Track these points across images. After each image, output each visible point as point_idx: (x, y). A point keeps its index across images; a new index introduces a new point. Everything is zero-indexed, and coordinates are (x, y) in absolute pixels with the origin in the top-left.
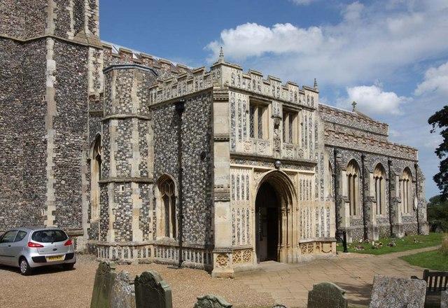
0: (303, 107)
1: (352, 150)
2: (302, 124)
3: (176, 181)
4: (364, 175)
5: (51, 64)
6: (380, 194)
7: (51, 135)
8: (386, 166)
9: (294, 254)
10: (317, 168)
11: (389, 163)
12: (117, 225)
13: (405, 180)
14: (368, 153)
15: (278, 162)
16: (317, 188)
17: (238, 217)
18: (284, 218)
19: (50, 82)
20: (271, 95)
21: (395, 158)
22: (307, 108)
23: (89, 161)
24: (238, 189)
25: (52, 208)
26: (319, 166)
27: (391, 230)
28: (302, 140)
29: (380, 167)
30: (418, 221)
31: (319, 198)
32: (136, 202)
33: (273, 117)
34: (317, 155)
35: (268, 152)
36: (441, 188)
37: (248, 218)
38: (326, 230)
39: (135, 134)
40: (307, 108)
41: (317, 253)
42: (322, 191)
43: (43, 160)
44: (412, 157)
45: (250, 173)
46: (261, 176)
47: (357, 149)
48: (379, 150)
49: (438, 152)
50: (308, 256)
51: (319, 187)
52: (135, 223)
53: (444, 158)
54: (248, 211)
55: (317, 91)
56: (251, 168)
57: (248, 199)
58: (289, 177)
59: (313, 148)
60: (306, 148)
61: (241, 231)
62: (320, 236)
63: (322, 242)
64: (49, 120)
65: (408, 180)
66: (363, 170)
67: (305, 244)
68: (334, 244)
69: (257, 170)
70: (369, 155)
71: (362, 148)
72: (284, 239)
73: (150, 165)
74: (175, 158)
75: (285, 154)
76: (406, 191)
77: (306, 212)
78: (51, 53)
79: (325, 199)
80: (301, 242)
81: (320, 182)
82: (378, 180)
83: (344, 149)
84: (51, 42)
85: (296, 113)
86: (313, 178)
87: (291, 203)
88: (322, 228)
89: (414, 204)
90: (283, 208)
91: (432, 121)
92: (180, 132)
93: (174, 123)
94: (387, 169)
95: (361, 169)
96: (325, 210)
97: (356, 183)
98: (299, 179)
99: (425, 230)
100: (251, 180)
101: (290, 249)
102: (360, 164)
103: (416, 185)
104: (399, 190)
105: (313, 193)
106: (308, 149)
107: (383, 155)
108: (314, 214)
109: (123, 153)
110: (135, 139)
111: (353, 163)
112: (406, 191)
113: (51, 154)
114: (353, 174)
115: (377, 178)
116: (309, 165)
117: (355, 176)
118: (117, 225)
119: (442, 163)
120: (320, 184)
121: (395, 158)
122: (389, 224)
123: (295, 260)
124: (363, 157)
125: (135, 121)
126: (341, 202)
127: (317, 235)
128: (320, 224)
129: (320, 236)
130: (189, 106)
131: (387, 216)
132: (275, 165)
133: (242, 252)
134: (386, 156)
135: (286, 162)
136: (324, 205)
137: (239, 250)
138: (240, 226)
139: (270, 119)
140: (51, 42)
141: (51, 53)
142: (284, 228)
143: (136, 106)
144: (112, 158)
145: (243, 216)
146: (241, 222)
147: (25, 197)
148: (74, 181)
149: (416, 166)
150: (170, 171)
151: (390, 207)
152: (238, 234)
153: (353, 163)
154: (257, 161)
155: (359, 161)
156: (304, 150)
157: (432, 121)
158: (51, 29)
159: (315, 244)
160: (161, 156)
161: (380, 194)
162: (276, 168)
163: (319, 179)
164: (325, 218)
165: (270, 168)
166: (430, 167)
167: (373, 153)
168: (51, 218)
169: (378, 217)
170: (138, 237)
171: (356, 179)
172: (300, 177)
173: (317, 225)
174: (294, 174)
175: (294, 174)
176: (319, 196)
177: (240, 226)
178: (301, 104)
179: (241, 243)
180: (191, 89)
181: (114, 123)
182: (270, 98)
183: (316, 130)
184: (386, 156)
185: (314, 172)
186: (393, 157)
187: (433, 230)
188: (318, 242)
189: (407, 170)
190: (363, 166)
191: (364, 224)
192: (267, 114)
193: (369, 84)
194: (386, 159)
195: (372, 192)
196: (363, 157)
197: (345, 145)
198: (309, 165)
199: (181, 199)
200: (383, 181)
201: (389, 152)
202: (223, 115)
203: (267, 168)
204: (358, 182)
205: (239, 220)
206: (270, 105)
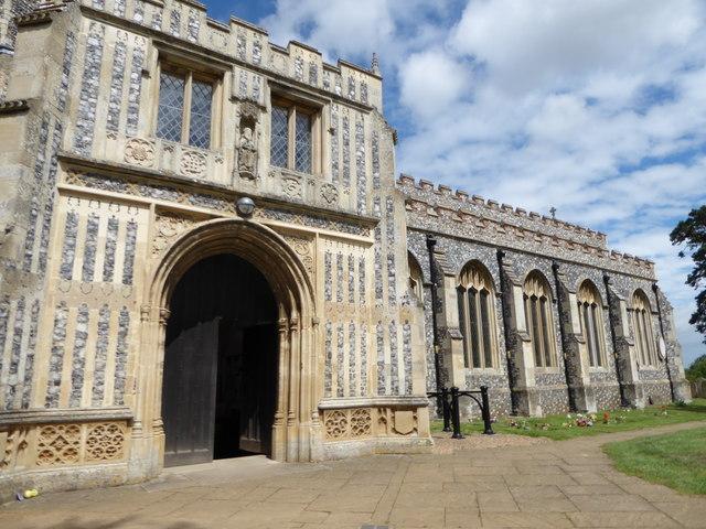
0: (336, 98)
1: (534, 255)
2: (332, 131)
4: (561, 296)
6: (596, 332)
8: (600, 285)
9: (304, 438)
10: (378, 232)
13: (638, 311)
14: (565, 261)
15: (247, 201)
16: (378, 276)
17: (82, 328)
18: (284, 344)
20: (232, 52)
21: (616, 273)
22: (348, 102)
24: (89, 253)
26: (383, 226)
27: (622, 393)
28: (335, 166)
29: (588, 285)
30: (669, 379)
31: (385, 301)
33: (234, 99)
34: (377, 201)
35: (219, 172)
37: (123, 335)
38: (402, 375)
40: (348, 102)
41: (379, 437)
42: (392, 284)
44: (645, 273)
45: (144, 217)
46: (182, 229)
47: (542, 253)
48: (585, 259)
49: (692, 280)
50: (349, 445)
51: (384, 273)
53: (701, 289)
54: (125, 314)
55: (377, 74)
56: (147, 205)
57: (128, 280)
58: (292, 245)
59: (369, 187)
60: (348, 184)
61: (89, 368)
62: (388, 391)
63: (394, 408)
65: (643, 311)
66: (558, 288)
67: (337, 411)
68: (424, 414)
69: (163, 212)
70: (566, 265)
71: (553, 252)
72: (282, 398)
76: (642, 329)
77: (347, 332)
79: (399, 301)
80: (325, 405)
81: (385, 262)
82: (589, 308)
83: (517, 251)
85: (317, 110)
86: (369, 254)
87: (299, 308)
88: (394, 373)
89: (659, 350)
90: (283, 319)
94: (603, 291)
95: (554, 287)
96: (400, 330)
97: (547, 312)
98: (320, 253)
101: (294, 424)
102: (551, 279)
103: (660, 319)
104: (627, 325)
105: (370, 289)
106: (354, 189)
107: (593, 267)
108: (371, 339)
111: (535, 276)
112: (642, 329)
114: (540, 294)
115: (586, 305)
117: (543, 300)
120: (385, 268)
121: (616, 273)
122: (616, 384)
123: (304, 454)
124: (555, 268)
126: (515, 342)
127: (381, 390)
128: (388, 361)
129: (388, 391)
131: (611, 369)
132: (237, 209)
133: (85, 432)
134: (599, 269)
136: (396, 317)
137: (73, 424)
138: (89, 352)
139: (228, 104)
142: (283, 370)
145: (104, 327)
146: (91, 343)
149: (655, 288)
152: (77, 377)
153: (535, 276)
154: (171, 189)
155: (548, 275)
156: (341, 189)
157: (676, 236)
159: (374, 414)
161: (596, 332)
162: (239, 214)
163: (384, 254)
164: (400, 345)
165: (216, 213)
166: (683, 303)
167: (574, 263)
169: (594, 372)
171: (547, 304)
172: (323, 246)
173: (381, 364)
174: (308, 237)
175: (308, 237)
176: (385, 293)
177: (89, 352)
178: (331, 90)
179: (86, 401)
182: (227, 58)
183: (375, 151)
184: (599, 269)
185: (371, 239)
186: (612, 272)
188: (381, 408)
189: (639, 293)
190: (557, 283)
191: (568, 382)
192: (223, 91)
195: (576, 326)
196: (555, 268)
197: (520, 245)
200: (599, 309)
201: (603, 263)
202: (34, 56)
203: (208, 211)
204: (551, 311)
205: (84, 336)
206: (228, 75)
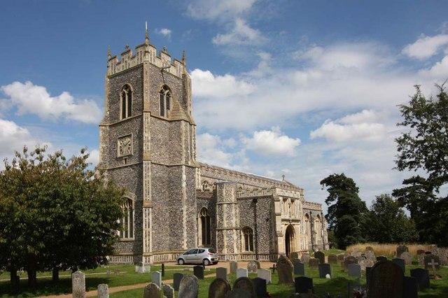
3: (253, 229)
4: (312, 221)
5: (184, 177)
7: (185, 208)
11: (311, 213)
12: (228, 246)
19: (184, 185)
23: (197, 219)
25: (186, 240)
32: (235, 237)
36: (329, 223)
39: (234, 210)
43: (181, 218)
52: (235, 245)
64: (184, 202)
73: (238, 222)
74: (253, 220)
75: (293, 218)
78: (184, 172)
84: (184, 167)
91: (327, 181)
92: (255, 210)
93: (252, 206)
98: (297, 227)
99: (327, 247)
100: (285, 228)
109: (229, 217)
110: (233, 212)
113: (185, 217)
116: (298, 221)
118: (228, 246)
119: (329, 208)
125: (233, 205)
130: (259, 201)
135: (293, 221)
140: (184, 167)
141: (184, 172)
143: (233, 199)
144: (225, 220)
147: (170, 235)
148: (192, 228)
150: (250, 224)
151: (312, 235)
158: (183, 162)
160: (244, 219)
168: (186, 245)
170: (236, 251)
180: (260, 194)
181: (225, 205)
187: (330, 247)
193: (269, 129)
194: (309, 211)
198: (298, 221)
199: (256, 235)
